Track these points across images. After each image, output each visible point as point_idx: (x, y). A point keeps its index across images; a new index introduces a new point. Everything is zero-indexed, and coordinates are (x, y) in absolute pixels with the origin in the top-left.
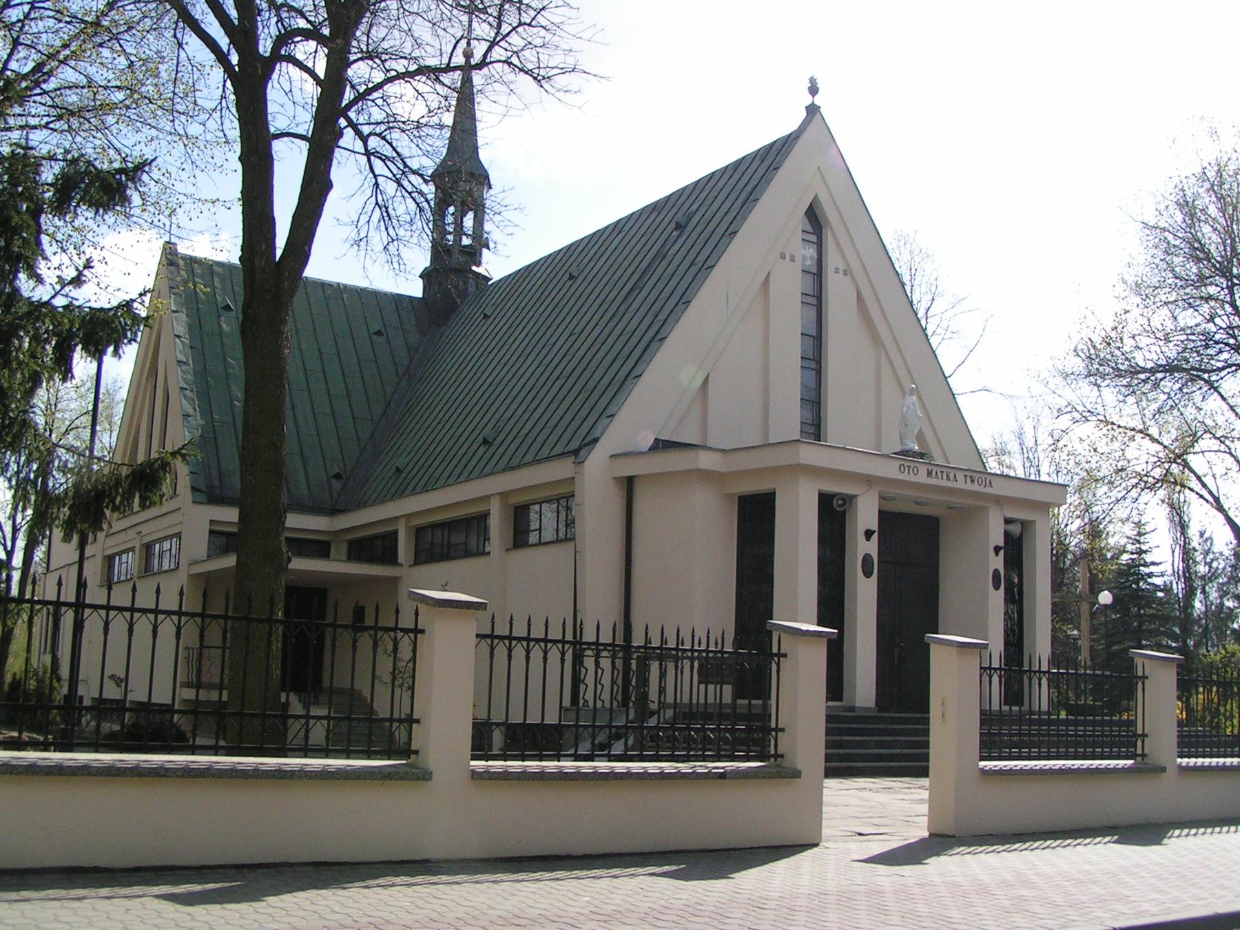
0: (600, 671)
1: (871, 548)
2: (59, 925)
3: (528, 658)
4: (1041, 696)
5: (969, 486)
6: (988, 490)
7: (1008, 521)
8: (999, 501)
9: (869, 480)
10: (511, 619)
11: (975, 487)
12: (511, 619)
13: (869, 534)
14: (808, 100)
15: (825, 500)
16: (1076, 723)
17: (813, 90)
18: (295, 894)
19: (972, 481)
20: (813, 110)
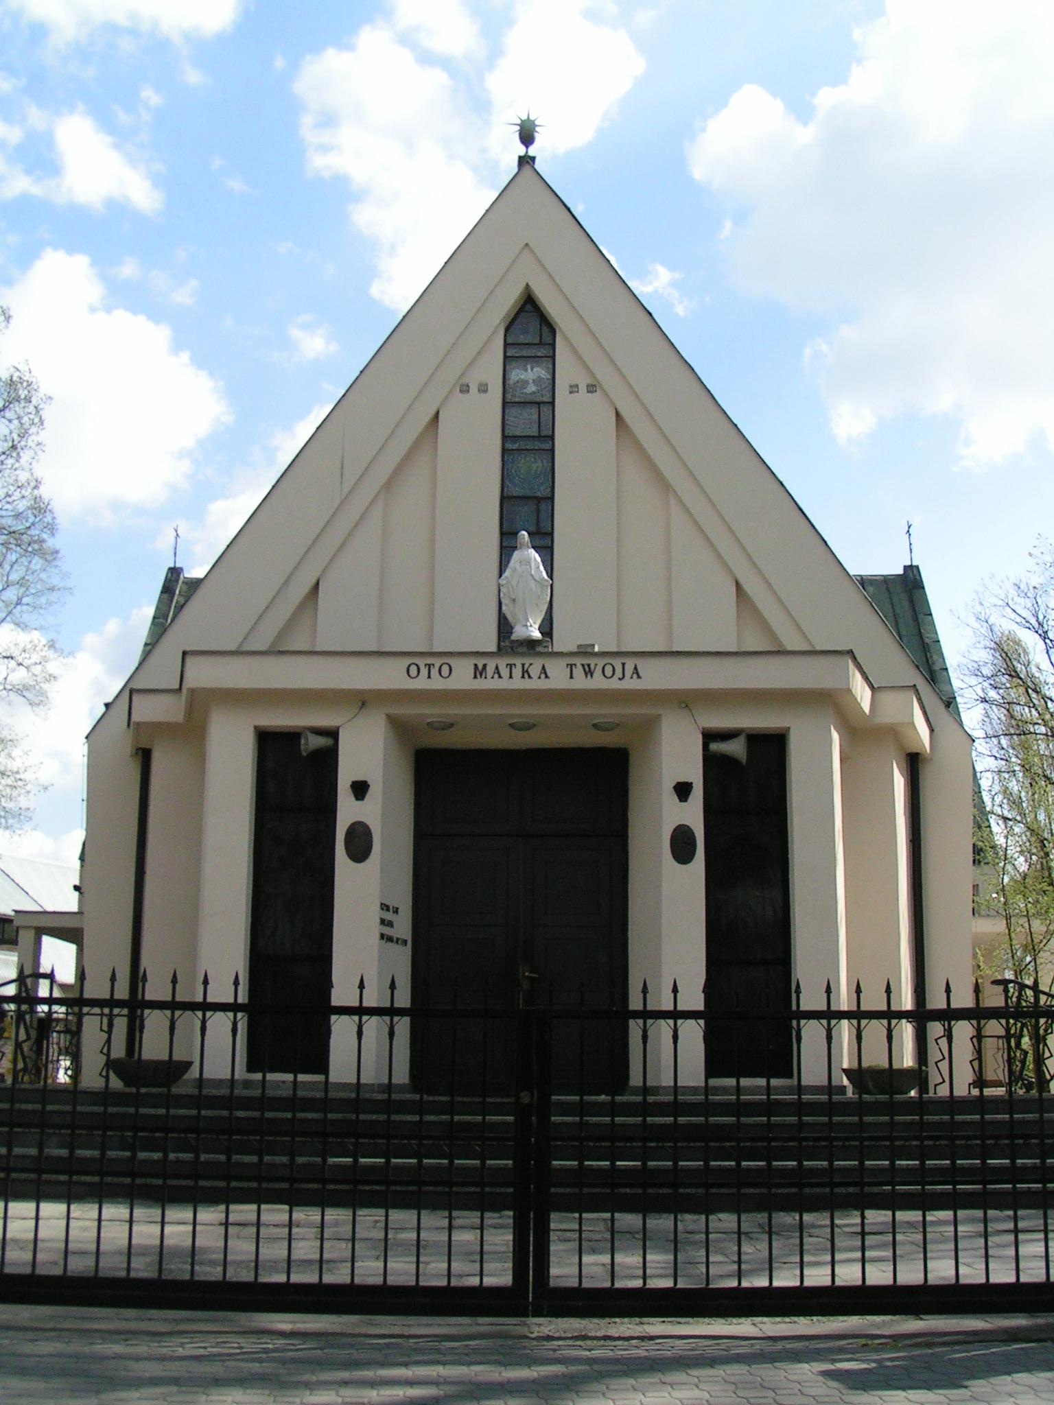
0: (105, 1051)
1: (692, 814)
2: (804, 1400)
3: (360, 1034)
4: (362, 1053)
5: (581, 682)
6: (630, 684)
7: (709, 737)
8: (685, 700)
9: (362, 700)
10: (948, 984)
11: (598, 682)
12: (948, 984)
13: (683, 790)
14: (521, 150)
15: (275, 748)
16: (136, 1100)
17: (527, 136)
18: (1018, 1376)
19: (589, 672)
20: (526, 161)
